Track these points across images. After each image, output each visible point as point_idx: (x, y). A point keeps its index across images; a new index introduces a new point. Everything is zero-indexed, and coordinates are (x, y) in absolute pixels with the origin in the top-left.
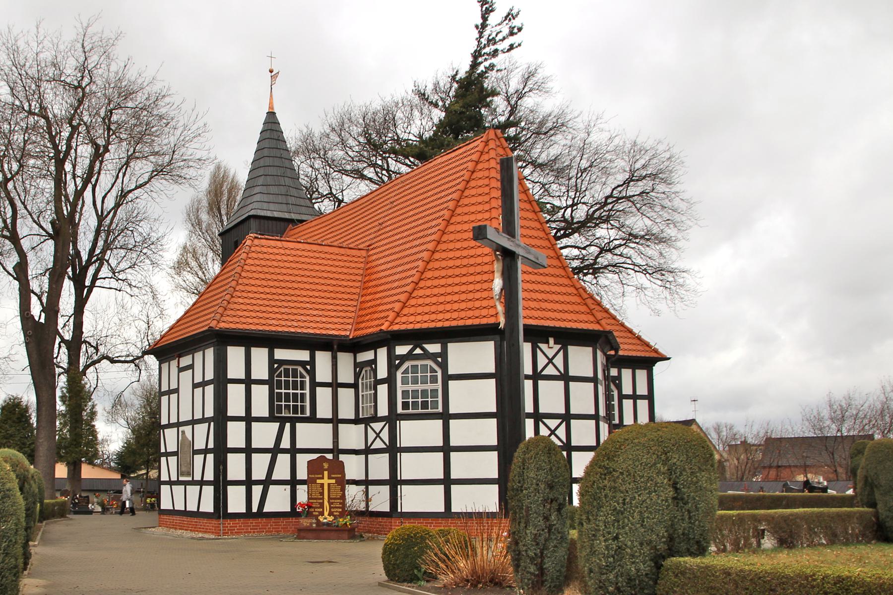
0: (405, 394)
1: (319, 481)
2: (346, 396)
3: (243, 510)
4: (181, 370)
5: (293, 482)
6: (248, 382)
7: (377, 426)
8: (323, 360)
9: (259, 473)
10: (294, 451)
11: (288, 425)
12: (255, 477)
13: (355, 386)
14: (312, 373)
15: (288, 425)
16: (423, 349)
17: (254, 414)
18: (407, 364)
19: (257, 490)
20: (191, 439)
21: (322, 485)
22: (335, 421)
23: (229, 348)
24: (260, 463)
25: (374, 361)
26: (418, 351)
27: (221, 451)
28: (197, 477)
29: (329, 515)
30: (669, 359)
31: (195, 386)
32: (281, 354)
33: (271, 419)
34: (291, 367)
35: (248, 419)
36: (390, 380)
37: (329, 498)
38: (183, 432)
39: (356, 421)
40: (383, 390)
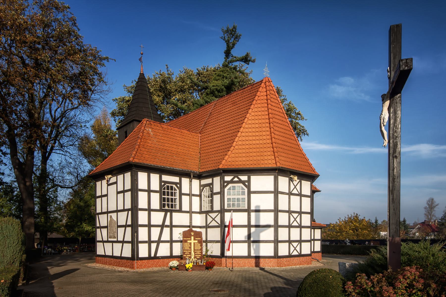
0: (229, 199)
1: (188, 241)
2: (196, 200)
3: (147, 255)
4: (109, 185)
5: (171, 242)
6: (149, 191)
7: (213, 215)
8: (185, 181)
9: (155, 237)
10: (171, 226)
11: (169, 214)
12: (152, 239)
13: (200, 196)
14: (180, 189)
15: (169, 214)
16: (238, 178)
17: (152, 207)
18: (230, 185)
19: (154, 246)
20: (116, 220)
21: (190, 243)
22: (190, 212)
23: (139, 173)
24: (155, 232)
25: (212, 184)
26: (236, 179)
27: (135, 226)
28: (120, 238)
29: (194, 258)
30: (320, 191)
31: (118, 193)
32: (166, 178)
33: (160, 210)
34: (170, 185)
35: (149, 210)
36: (222, 193)
37: (194, 250)
38: (111, 217)
39: (201, 212)
40: (217, 199)
